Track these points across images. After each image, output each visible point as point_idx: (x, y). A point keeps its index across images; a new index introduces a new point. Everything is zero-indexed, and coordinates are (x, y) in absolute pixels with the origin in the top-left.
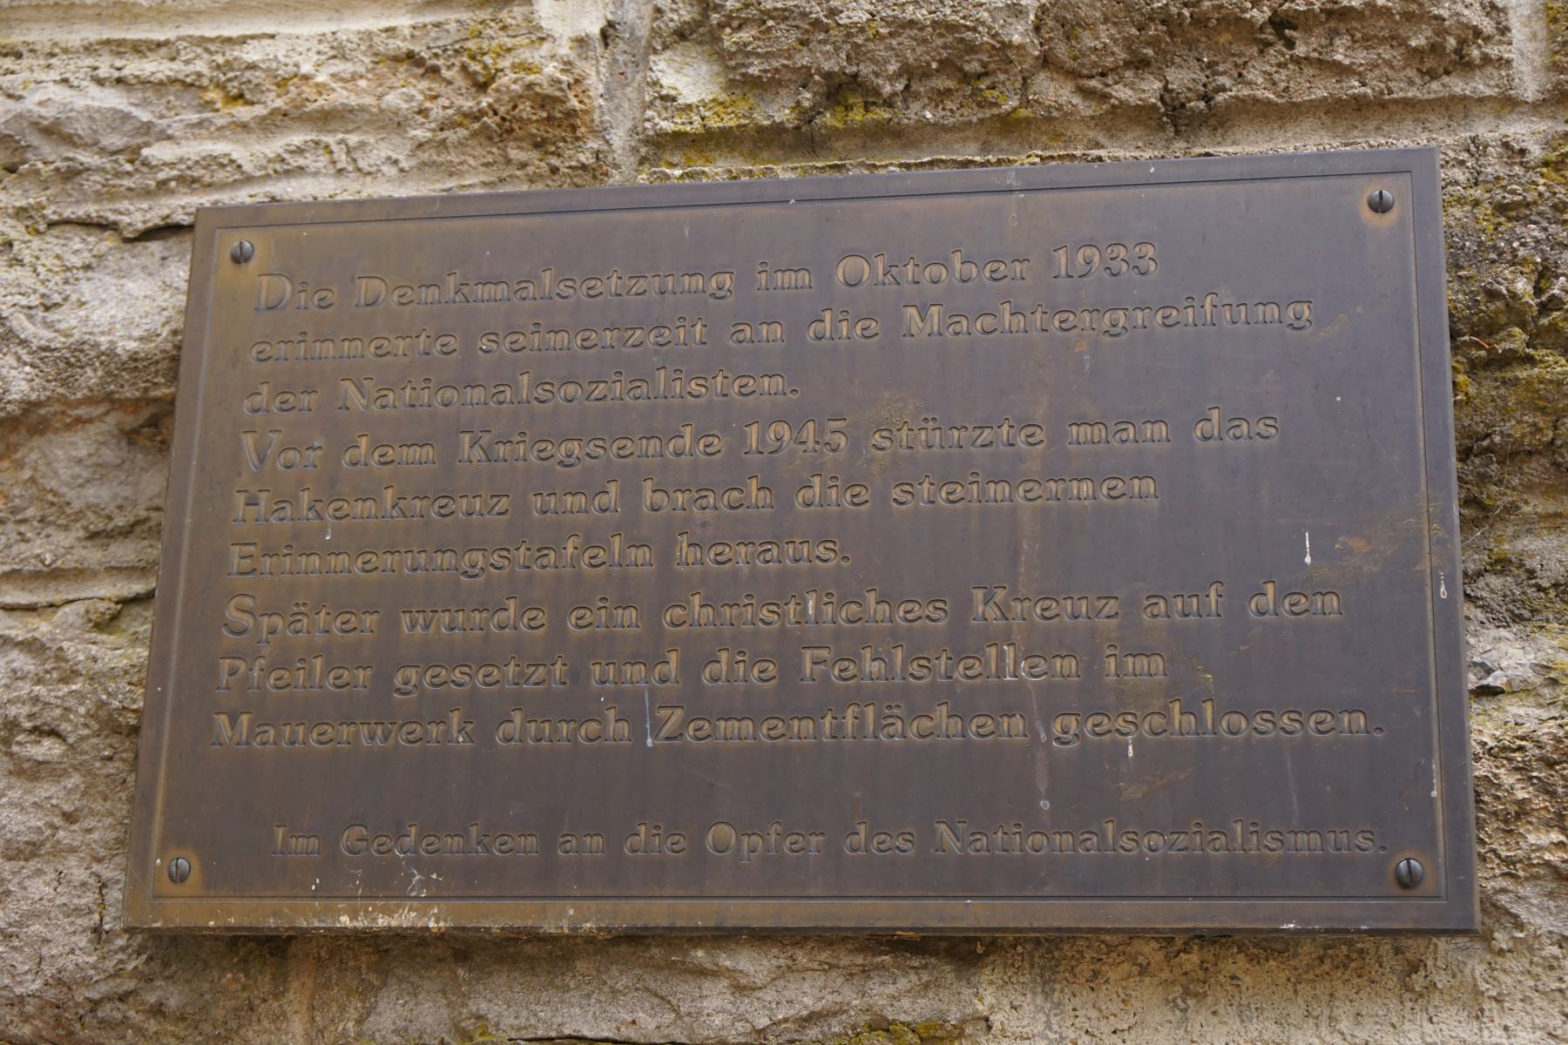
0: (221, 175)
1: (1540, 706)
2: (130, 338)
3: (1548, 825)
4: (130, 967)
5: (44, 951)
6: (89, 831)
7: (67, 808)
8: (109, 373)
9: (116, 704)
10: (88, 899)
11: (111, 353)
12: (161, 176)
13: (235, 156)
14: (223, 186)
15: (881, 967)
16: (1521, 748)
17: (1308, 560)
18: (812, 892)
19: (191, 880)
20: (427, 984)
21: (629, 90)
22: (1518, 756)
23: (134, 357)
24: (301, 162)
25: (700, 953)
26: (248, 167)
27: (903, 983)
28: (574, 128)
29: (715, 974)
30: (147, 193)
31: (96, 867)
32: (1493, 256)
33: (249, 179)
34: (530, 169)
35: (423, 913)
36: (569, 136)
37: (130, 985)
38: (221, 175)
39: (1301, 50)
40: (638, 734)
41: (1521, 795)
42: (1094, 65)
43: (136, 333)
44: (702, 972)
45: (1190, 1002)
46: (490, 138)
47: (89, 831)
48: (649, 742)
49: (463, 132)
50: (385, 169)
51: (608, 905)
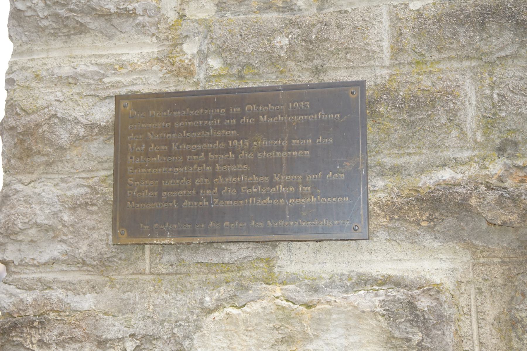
0: (120, 85)
1: (384, 193)
2: (104, 122)
3: (384, 218)
4: (114, 251)
5: (97, 248)
6: (104, 224)
7: (100, 220)
8: (100, 130)
9: (107, 199)
10: (105, 238)
11: (100, 125)
12: (107, 85)
13: (122, 81)
14: (120, 88)
15: (258, 248)
16: (379, 203)
17: (338, 167)
18: (244, 234)
19: (125, 235)
20: (172, 253)
21: (203, 65)
22: (378, 204)
23: (105, 126)
24: (136, 82)
25: (224, 246)
26: (125, 83)
27: (262, 251)
28: (192, 74)
29: (227, 250)
30: (104, 89)
31: (106, 231)
32: (377, 102)
33: (125, 86)
34: (184, 83)
35: (170, 240)
36: (191, 75)
37: (115, 254)
38: (120, 85)
39: (340, 56)
40: (210, 204)
41: (378, 212)
42: (299, 60)
43: (105, 121)
44: (224, 249)
45: (318, 252)
46: (175, 76)
47: (104, 224)
48: (212, 206)
49: (169, 75)
50: (153, 83)
51: (205, 238)
